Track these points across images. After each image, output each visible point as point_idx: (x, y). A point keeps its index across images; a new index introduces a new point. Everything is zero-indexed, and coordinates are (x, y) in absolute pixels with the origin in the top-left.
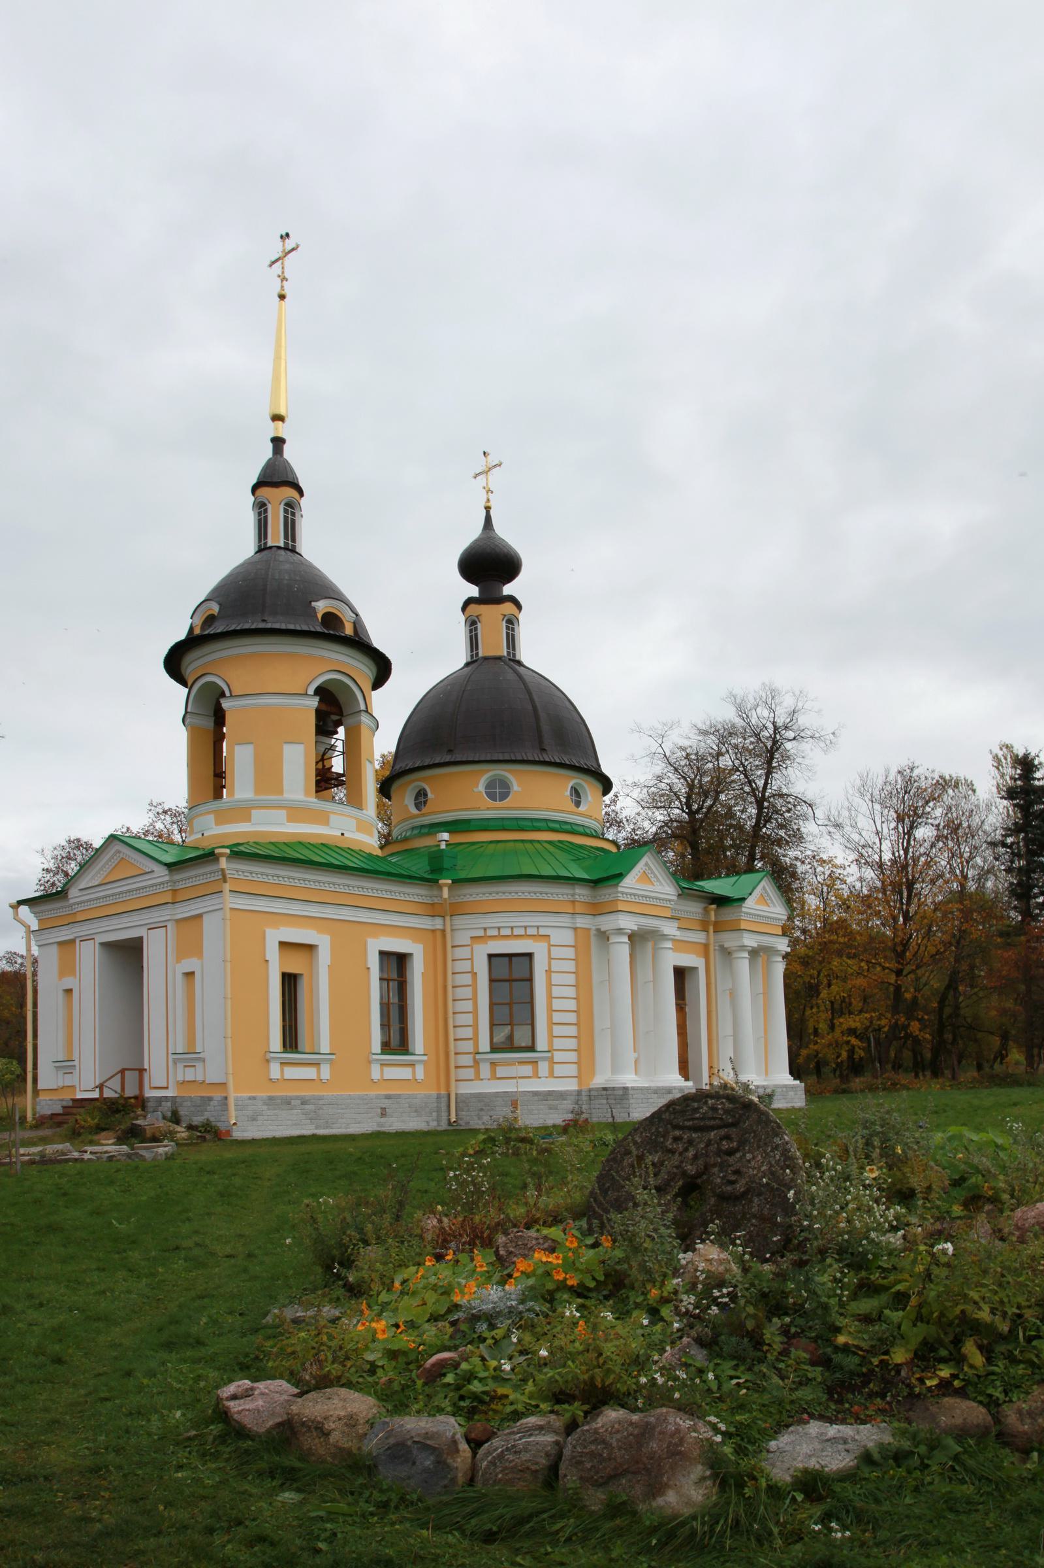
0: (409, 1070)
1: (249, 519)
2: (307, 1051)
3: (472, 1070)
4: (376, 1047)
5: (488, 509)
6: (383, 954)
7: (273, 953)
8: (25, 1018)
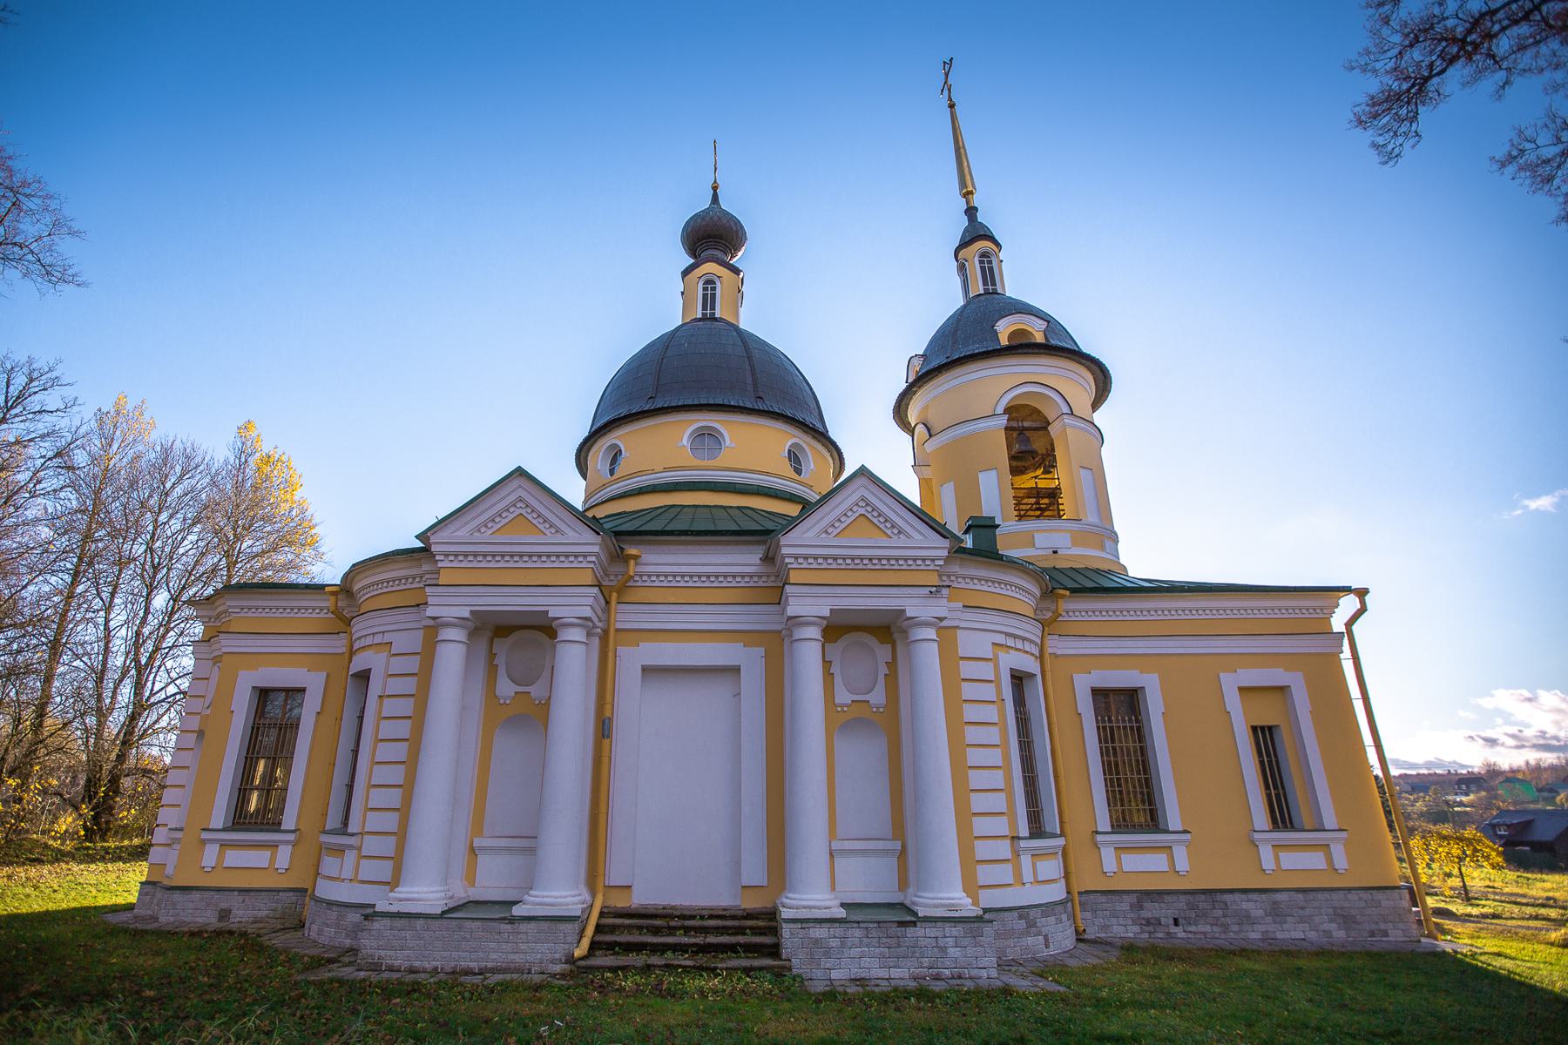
0: (267, 853)
1: (957, 281)
2: (1306, 828)
3: (1008, 867)
4: (1104, 823)
5: (715, 189)
6: (1099, 694)
7: (1233, 702)
8: (1051, 792)
